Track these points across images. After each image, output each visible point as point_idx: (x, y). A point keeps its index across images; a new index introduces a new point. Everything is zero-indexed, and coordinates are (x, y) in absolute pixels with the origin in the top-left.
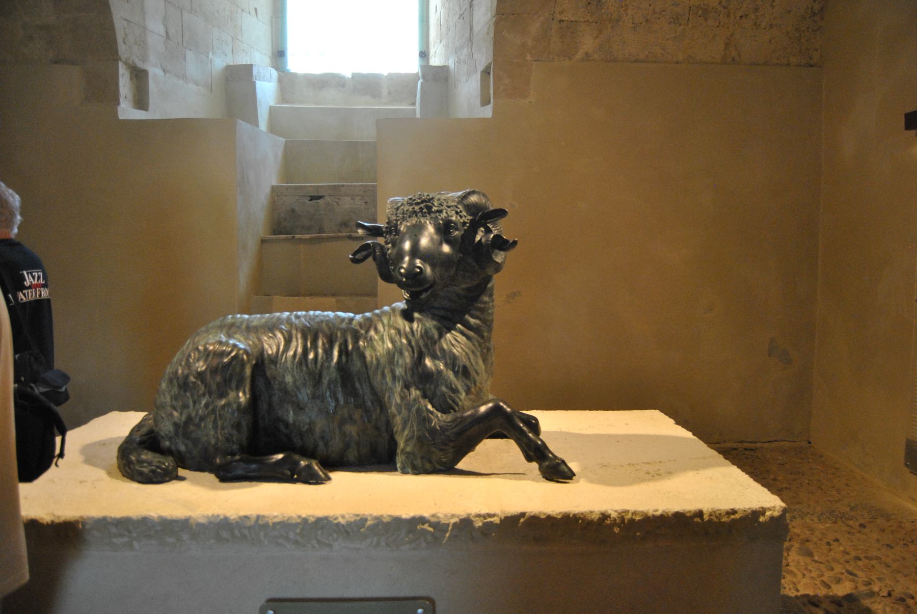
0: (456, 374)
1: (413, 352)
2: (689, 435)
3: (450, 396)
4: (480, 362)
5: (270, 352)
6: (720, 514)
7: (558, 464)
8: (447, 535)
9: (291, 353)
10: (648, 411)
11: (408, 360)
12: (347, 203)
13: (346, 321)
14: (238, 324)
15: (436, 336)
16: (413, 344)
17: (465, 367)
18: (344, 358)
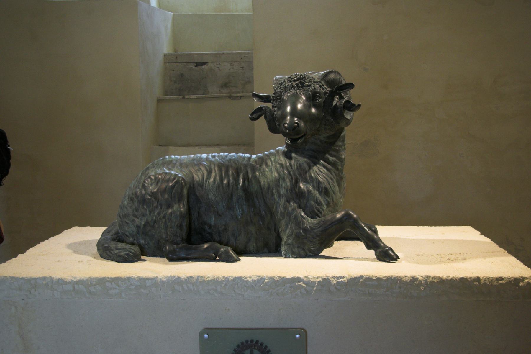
0: (320, 193)
1: (292, 178)
2: (489, 240)
3: (316, 208)
4: (337, 187)
5: (197, 179)
6: (492, 280)
7: (387, 250)
8: (315, 289)
9: (211, 180)
10: (463, 227)
11: (289, 184)
12: (226, 68)
13: (246, 159)
14: (174, 162)
15: (307, 169)
16: (292, 173)
17: (326, 189)
18: (246, 182)
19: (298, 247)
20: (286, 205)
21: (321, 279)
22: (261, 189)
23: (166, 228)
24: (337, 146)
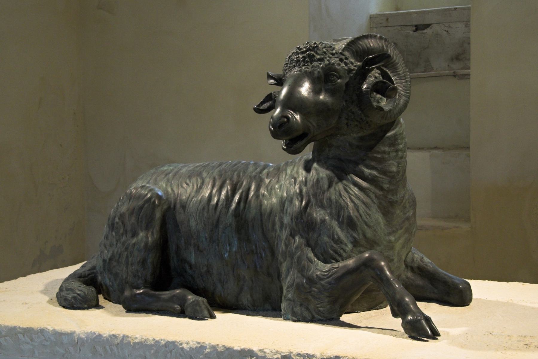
0: (341, 224)
15: (326, 186)
17: (350, 218)
19: (301, 305)
20: (289, 241)
21: (279, 356)
22: (261, 215)
23: (127, 264)
24: (378, 153)
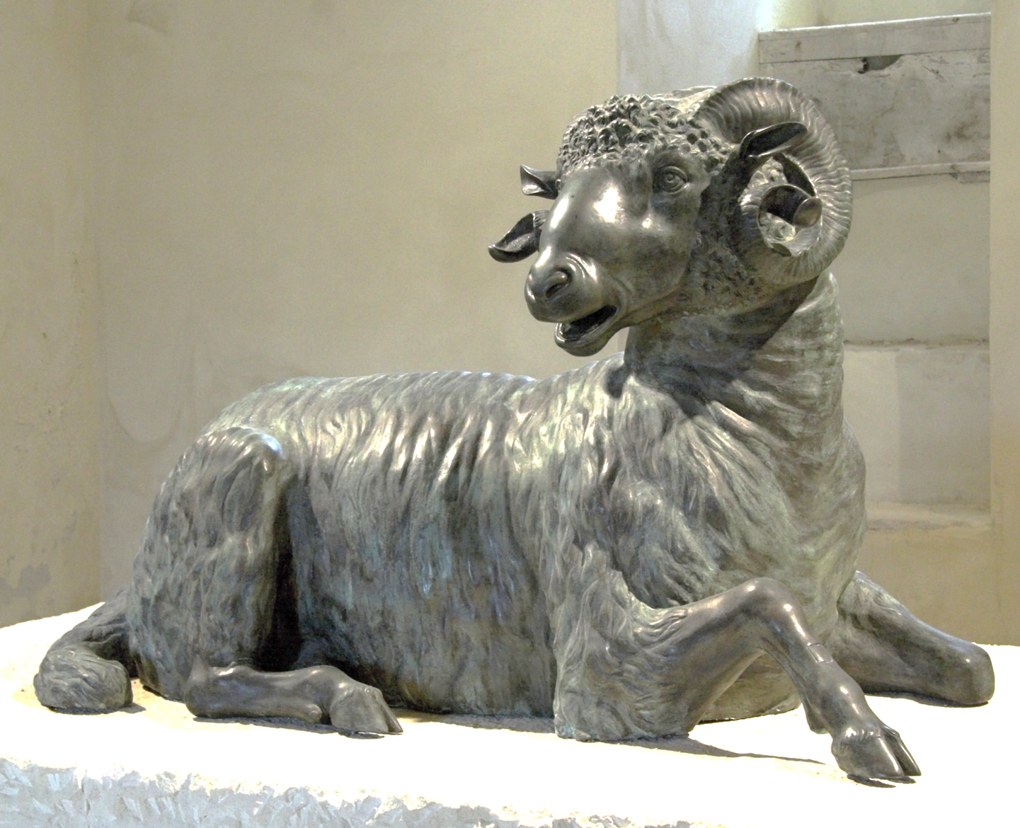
0: (690, 516)
15: (657, 430)
19: (599, 703)
20: (571, 555)
22: (507, 495)
23: (198, 608)
24: (778, 352)
